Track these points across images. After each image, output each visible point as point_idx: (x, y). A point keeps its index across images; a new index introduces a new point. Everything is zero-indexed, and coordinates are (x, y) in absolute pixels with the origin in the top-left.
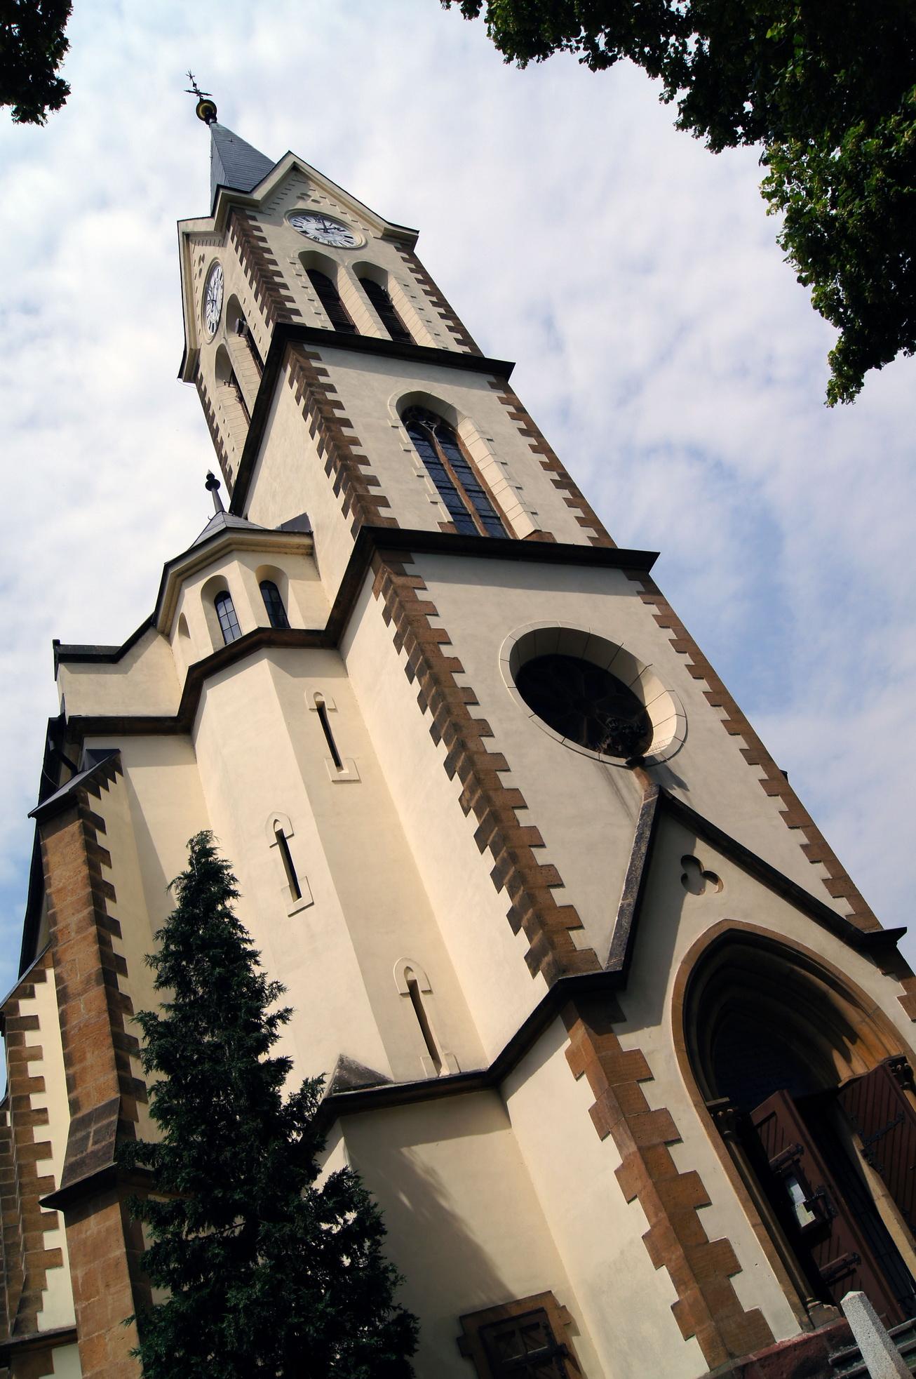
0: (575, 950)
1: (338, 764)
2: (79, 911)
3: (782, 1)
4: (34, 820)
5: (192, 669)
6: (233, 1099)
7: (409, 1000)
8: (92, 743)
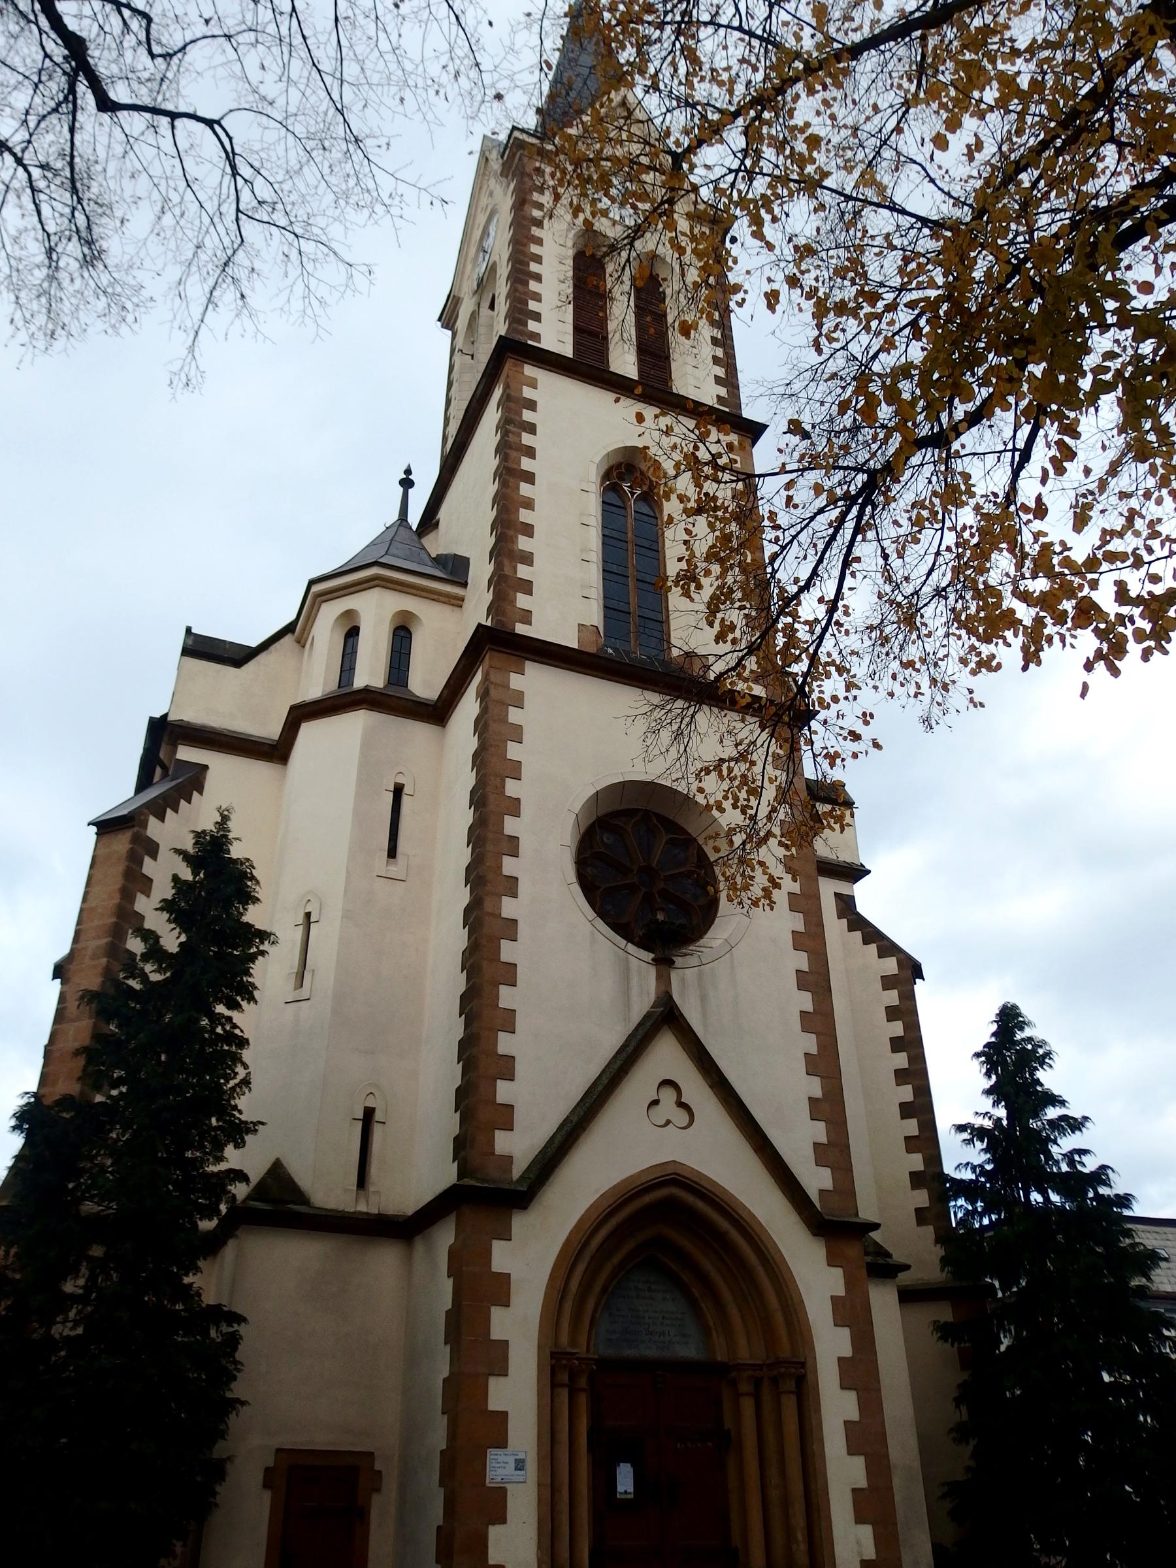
0: (493, 1153)
1: (392, 853)
2: (99, 938)
3: (1171, 108)
4: (94, 829)
5: (293, 709)
6: (218, 1120)
7: (359, 1125)
8: (186, 753)
